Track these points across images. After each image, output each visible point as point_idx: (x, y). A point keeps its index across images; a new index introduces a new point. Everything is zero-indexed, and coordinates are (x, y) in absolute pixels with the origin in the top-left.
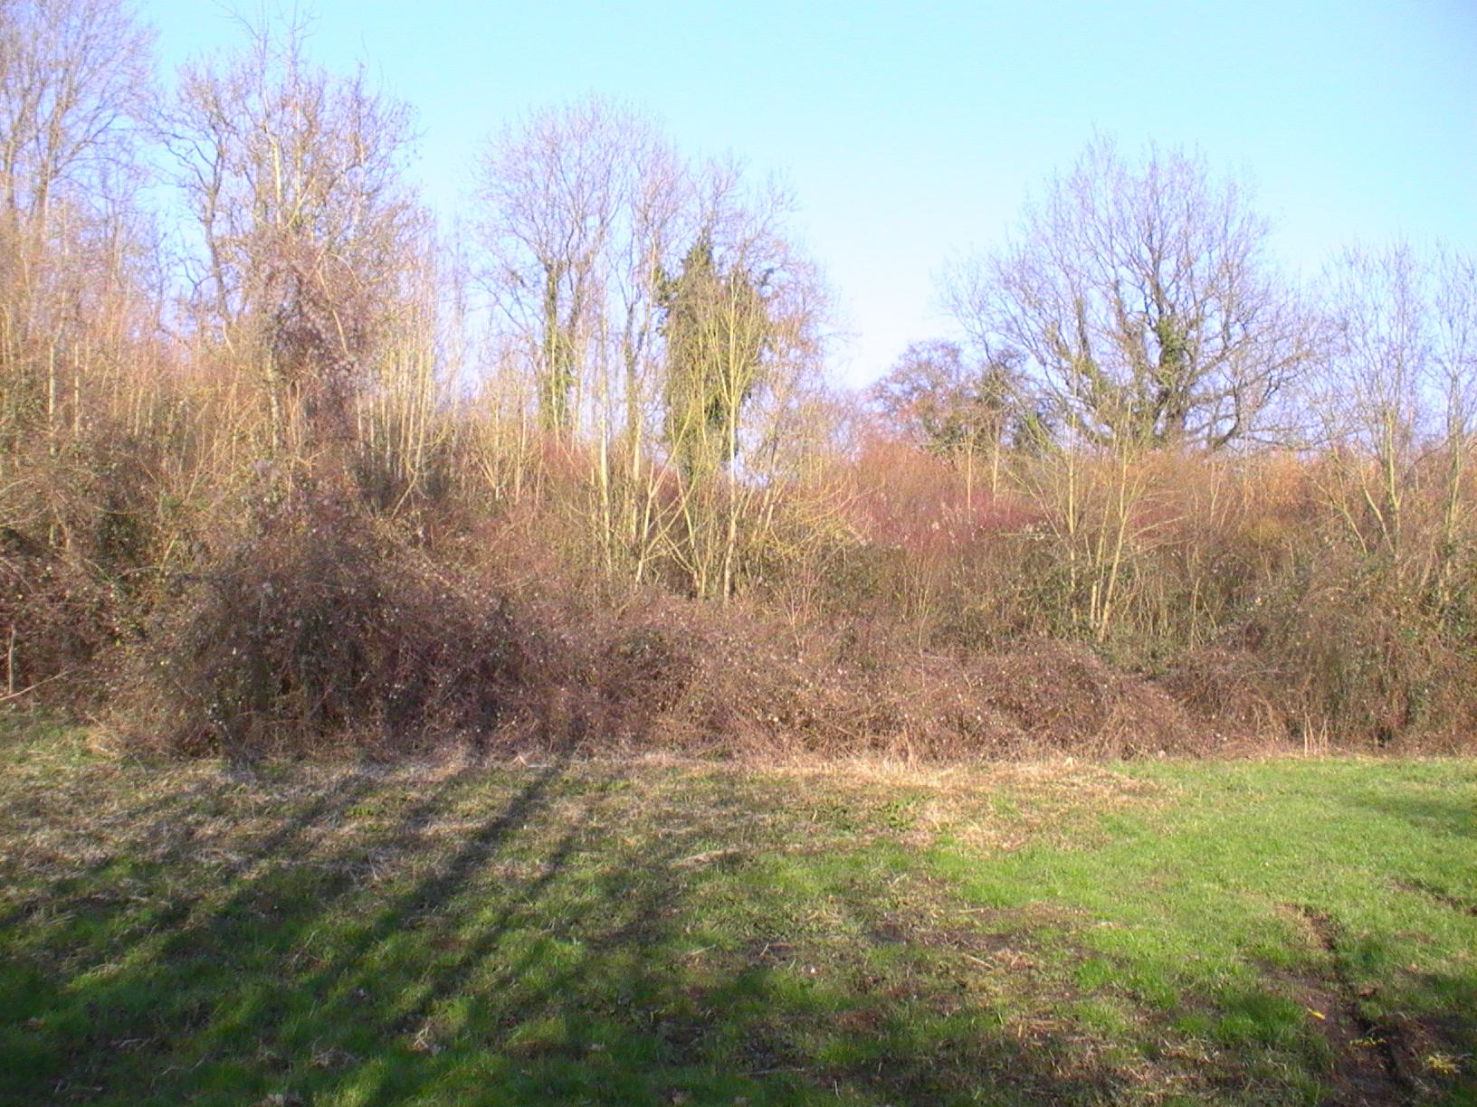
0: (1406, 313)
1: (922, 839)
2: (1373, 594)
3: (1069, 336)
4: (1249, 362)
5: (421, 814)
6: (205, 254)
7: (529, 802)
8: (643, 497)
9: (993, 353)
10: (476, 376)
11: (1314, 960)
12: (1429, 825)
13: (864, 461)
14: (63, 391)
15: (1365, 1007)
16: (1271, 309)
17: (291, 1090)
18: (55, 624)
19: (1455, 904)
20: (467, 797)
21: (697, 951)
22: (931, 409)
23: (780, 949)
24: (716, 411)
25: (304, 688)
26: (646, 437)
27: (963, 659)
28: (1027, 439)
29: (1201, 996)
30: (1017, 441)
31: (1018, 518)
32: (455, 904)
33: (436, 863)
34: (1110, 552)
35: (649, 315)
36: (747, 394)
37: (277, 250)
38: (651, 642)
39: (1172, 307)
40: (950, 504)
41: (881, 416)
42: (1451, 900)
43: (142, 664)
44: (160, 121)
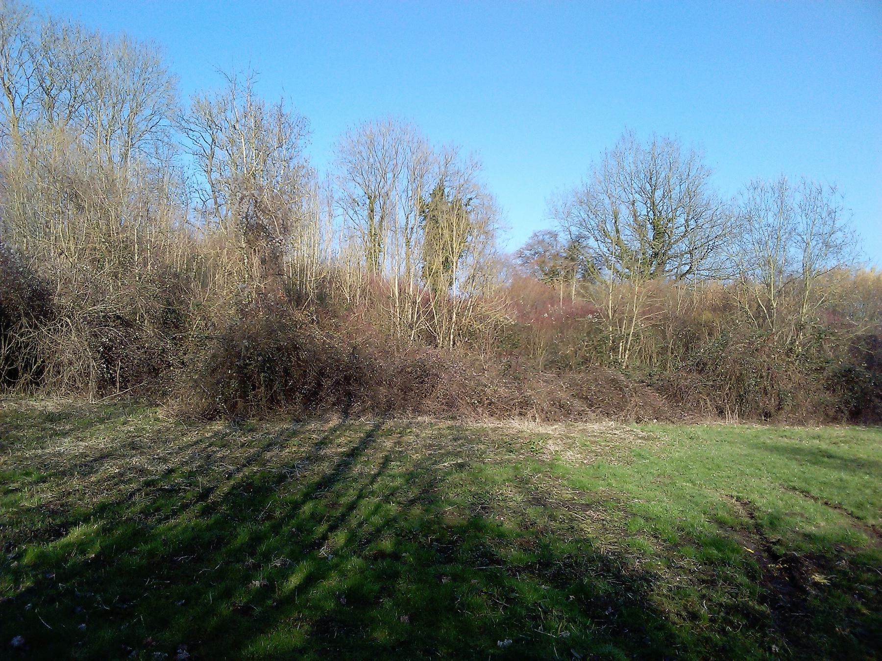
0: (783, 210)
1: (547, 458)
2: (762, 347)
3: (609, 227)
4: (698, 237)
5: (322, 443)
6: (208, 187)
7: (369, 439)
8: (414, 302)
9: (573, 236)
10: (338, 247)
11: (744, 523)
12: (796, 459)
13: (513, 286)
14: (141, 251)
15: (775, 548)
16: (710, 212)
17: (263, 579)
18: (140, 359)
19: (816, 499)
20: (339, 437)
21: (449, 508)
22: (543, 262)
23: (485, 508)
24: (446, 264)
25: (263, 388)
26: (415, 276)
27: (559, 375)
28: (589, 274)
29: (688, 537)
30: (584, 276)
31: (586, 311)
32: (338, 486)
33: (326, 468)
34: (629, 327)
35: (415, 220)
36: (460, 256)
37: (245, 187)
38: (420, 367)
39: (660, 212)
40: (552, 306)
41: (521, 265)
42: (813, 497)
43: (184, 377)
44: (183, 123)
